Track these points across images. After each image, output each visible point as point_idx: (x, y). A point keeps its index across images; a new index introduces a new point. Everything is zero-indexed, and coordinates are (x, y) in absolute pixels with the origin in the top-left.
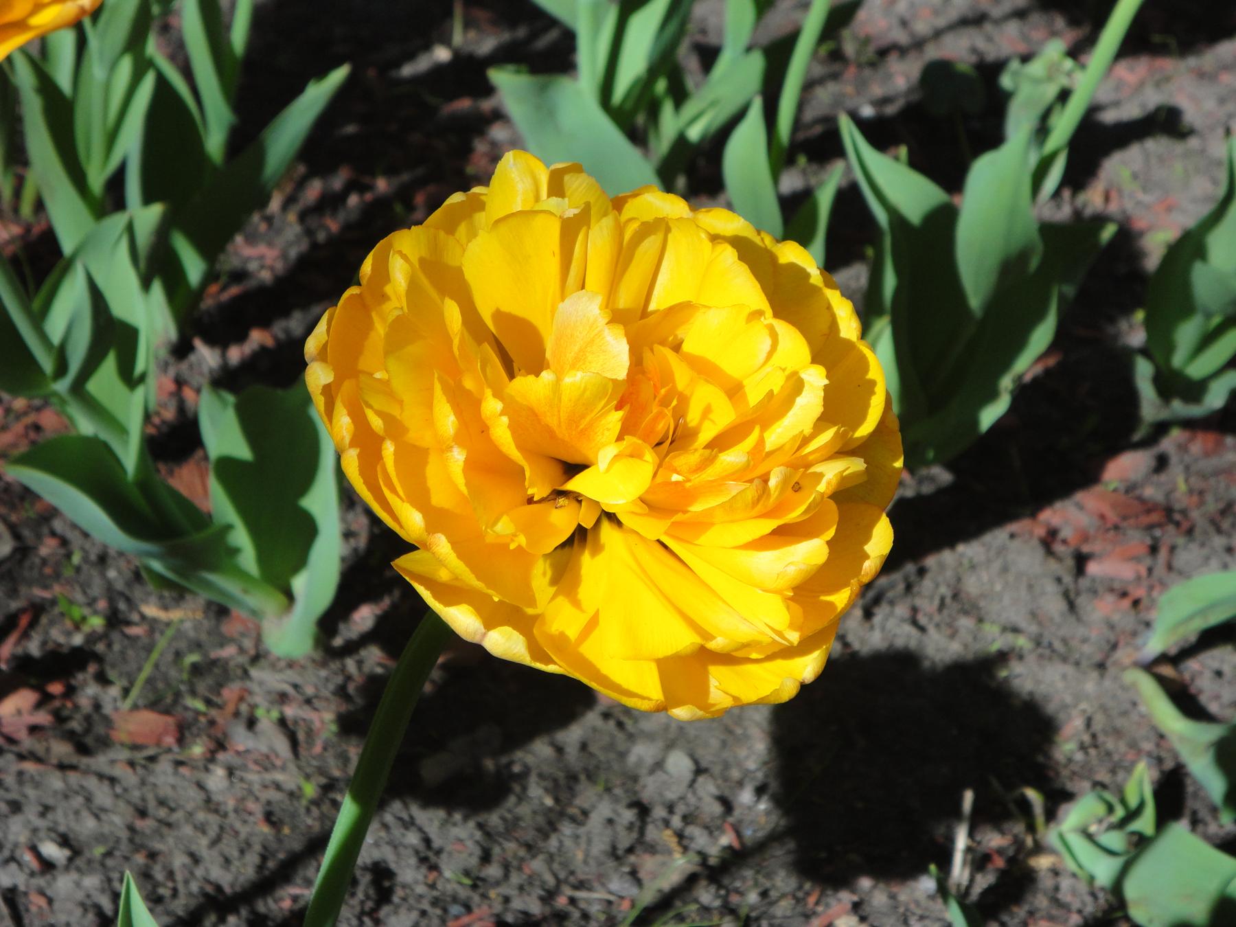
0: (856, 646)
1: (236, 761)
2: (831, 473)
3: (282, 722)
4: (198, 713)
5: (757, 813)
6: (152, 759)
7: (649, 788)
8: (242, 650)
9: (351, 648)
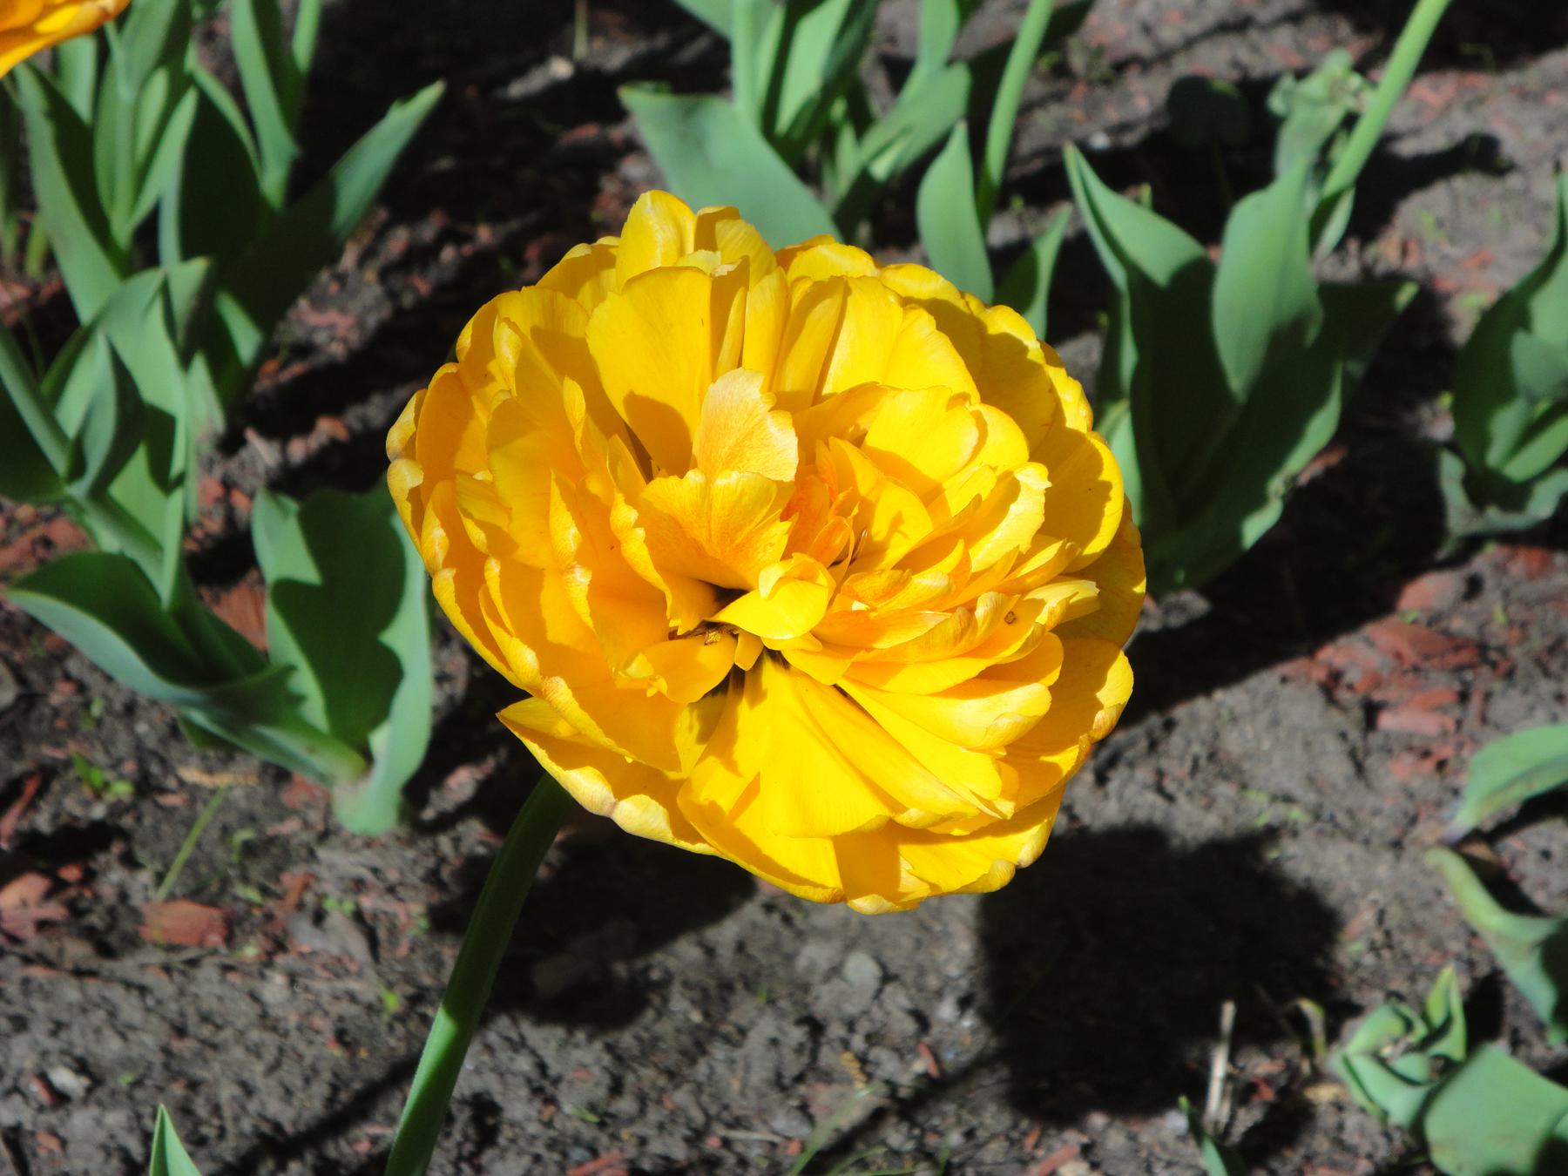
0: (1086, 819)
1: (300, 965)
2: (1055, 600)
3: (358, 916)
4: (251, 904)
5: (961, 1031)
6: (193, 963)
7: (824, 1000)
8: (306, 825)
9: (446, 822)
